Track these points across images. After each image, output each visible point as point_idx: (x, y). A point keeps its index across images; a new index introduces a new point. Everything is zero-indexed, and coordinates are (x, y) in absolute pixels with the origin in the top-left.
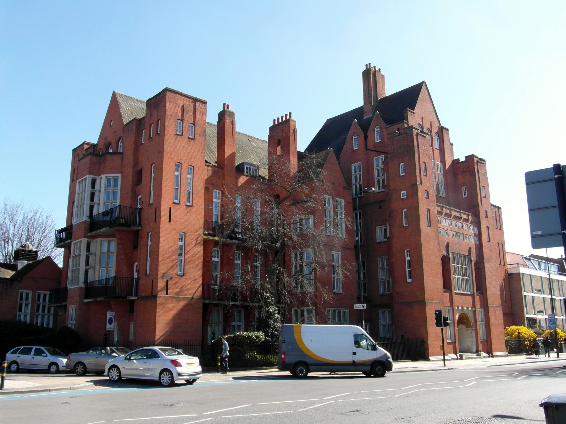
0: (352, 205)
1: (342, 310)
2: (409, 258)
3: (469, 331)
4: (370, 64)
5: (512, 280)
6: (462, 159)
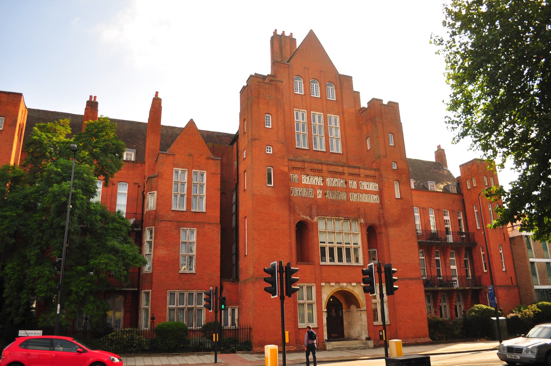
0: (219, 176)
1: (195, 292)
2: (483, 253)
3: (359, 313)
4: (276, 30)
5: (515, 245)
6: (366, 106)
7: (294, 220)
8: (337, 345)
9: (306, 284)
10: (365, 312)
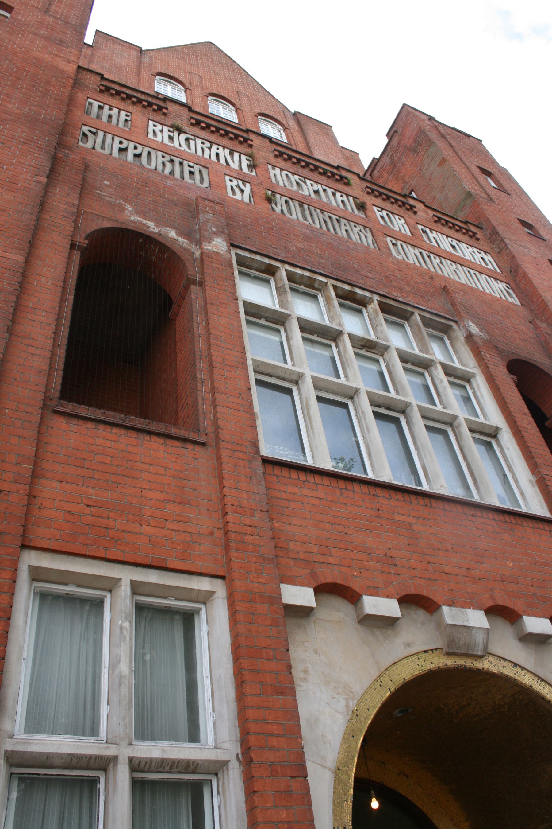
7: (78, 214)
9: (127, 576)
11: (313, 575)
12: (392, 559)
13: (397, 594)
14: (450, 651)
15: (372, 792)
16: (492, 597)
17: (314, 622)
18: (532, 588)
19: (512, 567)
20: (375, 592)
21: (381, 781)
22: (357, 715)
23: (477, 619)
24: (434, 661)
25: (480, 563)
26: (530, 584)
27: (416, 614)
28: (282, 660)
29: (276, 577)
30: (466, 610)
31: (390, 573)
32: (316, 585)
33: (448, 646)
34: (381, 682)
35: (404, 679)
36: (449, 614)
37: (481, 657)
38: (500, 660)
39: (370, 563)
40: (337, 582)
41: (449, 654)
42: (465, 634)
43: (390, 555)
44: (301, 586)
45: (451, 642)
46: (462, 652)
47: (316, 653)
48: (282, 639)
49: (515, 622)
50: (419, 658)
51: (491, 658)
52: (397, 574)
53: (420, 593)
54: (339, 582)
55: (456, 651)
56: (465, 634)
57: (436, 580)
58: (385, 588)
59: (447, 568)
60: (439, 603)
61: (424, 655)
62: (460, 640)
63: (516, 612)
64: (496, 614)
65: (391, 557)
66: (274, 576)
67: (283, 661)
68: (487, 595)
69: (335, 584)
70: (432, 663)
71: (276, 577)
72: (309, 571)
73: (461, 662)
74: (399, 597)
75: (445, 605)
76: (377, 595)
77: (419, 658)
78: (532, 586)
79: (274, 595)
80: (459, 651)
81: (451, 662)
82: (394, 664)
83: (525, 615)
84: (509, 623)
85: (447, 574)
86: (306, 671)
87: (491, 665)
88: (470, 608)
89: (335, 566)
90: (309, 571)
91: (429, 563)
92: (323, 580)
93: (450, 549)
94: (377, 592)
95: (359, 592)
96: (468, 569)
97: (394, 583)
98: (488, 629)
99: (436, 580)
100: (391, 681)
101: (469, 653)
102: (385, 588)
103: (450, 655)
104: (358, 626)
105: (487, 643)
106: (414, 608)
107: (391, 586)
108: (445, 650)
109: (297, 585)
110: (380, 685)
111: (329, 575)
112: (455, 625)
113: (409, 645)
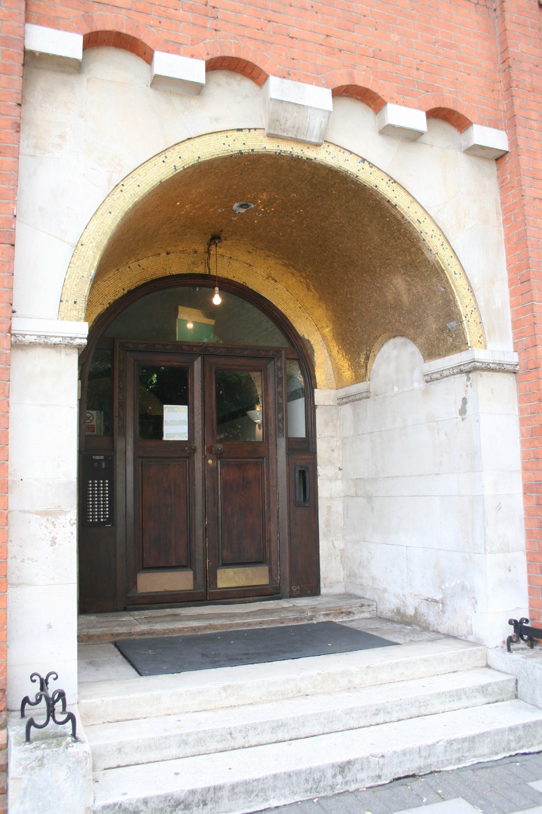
8: (196, 746)
10: (506, 385)
11: (88, 18)
12: (214, 10)
13: (208, 54)
14: (272, 132)
15: (217, 289)
16: (351, 75)
17: (88, 81)
18: (415, 72)
19: (397, 43)
20: (174, 48)
21: (244, 283)
22: (122, 191)
23: (319, 97)
24: (390, 190)
25: (349, 30)
26: (415, 67)
27: (239, 85)
28: (7, 115)
29: (20, 14)
30: (305, 85)
31: (205, 27)
32: (88, 31)
33: (270, 127)
34: (166, 157)
35: (199, 157)
36: (276, 86)
37: (318, 145)
38: (344, 153)
39: (177, 12)
40: (121, 31)
41: (271, 136)
42: (295, 114)
43: (213, 5)
44: (66, 30)
45: (274, 121)
46: (290, 135)
47: (82, 117)
48: (13, 90)
49: (379, 111)
50: (227, 136)
51: (332, 148)
52: (216, 30)
53: (242, 57)
54: (124, 31)
55: (280, 133)
56: (295, 114)
57: (272, 43)
58: (192, 45)
59: (294, 31)
60: (267, 73)
61: (236, 133)
62: (286, 121)
63: (380, 97)
64: (357, 99)
65: (214, 7)
66: (18, 11)
67: (9, 117)
68: (344, 71)
69: (119, 34)
70: (244, 144)
71: (20, 14)
72: (82, 13)
73: (286, 148)
74: (208, 58)
75: (274, 75)
76: (177, 52)
77: (227, 136)
78: (418, 69)
79: (13, 36)
80: (285, 134)
81: (272, 147)
82: (189, 139)
83: (391, 102)
84: (371, 111)
85: (292, 38)
86: (62, 137)
87: (328, 156)
88: (312, 84)
89: (123, 11)
90: (82, 13)
91: (269, 21)
92: (99, 26)
93: (308, 7)
94: (178, 49)
95: (151, 46)
96: (327, 36)
97: (208, 40)
98: (330, 112)
99: (272, 43)
100: (180, 157)
101: (299, 138)
102: (192, 45)
103: (273, 138)
104: (150, 91)
105: (326, 129)
106: (239, 77)
107: (201, 43)
108: (266, 131)
109: (59, 29)
110: (164, 162)
111: (108, 21)
112: (282, 101)
113: (217, 120)
